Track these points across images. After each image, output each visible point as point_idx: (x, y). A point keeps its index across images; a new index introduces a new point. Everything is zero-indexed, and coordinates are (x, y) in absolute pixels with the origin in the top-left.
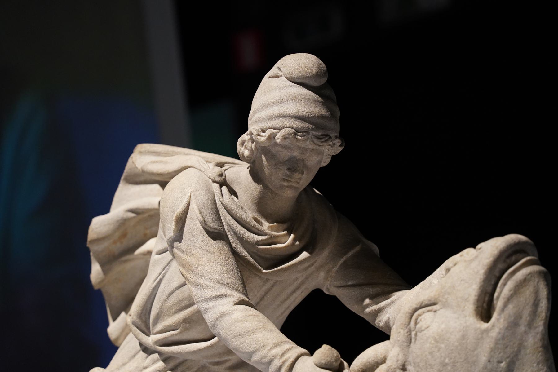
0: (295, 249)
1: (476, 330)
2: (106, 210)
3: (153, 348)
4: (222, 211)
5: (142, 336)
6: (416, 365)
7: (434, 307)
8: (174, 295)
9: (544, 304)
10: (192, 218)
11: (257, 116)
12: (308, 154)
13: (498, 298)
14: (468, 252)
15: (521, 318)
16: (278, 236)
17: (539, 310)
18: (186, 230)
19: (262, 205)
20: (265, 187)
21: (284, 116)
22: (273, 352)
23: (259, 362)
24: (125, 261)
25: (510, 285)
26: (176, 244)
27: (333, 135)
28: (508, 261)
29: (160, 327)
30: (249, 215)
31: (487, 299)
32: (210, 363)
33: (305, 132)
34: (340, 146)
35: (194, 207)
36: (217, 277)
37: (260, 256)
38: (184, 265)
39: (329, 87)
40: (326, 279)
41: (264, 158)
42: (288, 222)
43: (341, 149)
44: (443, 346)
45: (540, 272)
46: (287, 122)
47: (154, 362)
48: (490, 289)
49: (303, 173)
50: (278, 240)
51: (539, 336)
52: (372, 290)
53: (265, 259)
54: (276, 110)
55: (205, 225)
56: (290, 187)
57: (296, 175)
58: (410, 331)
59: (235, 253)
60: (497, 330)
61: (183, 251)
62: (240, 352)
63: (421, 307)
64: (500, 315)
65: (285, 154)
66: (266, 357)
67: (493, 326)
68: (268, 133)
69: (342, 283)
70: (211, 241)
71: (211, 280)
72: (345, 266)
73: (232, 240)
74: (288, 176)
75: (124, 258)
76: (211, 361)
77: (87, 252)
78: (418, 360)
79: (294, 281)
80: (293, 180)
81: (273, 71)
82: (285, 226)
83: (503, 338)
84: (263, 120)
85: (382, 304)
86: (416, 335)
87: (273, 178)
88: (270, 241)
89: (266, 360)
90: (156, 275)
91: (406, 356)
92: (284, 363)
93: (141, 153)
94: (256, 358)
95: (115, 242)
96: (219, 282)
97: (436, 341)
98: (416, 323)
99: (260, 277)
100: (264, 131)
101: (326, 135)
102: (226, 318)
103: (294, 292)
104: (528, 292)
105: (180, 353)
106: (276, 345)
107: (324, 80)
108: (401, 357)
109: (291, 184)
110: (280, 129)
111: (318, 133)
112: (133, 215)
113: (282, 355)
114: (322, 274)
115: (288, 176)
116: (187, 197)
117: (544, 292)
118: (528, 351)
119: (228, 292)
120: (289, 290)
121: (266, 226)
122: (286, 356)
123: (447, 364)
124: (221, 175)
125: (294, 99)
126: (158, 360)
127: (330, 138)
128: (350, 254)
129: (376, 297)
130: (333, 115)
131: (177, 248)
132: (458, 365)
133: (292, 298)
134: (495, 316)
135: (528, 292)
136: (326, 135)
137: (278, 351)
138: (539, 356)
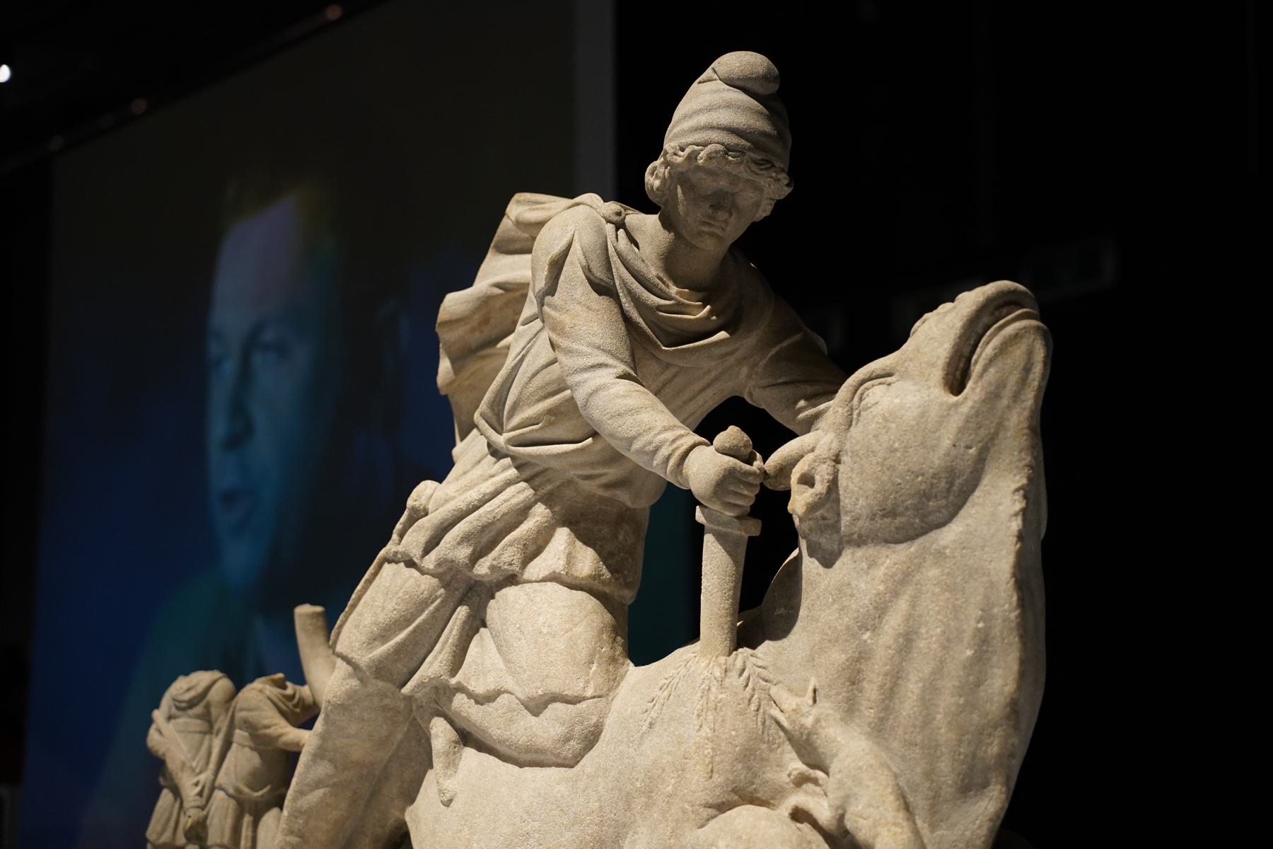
0: (710, 326)
1: (941, 404)
2: (467, 281)
3: (505, 451)
4: (615, 259)
5: (491, 432)
6: (855, 454)
7: (889, 379)
8: (539, 376)
9: (1038, 369)
10: (572, 263)
11: (675, 130)
12: (741, 186)
13: (976, 362)
14: (946, 306)
15: (1005, 387)
16: (689, 305)
17: (1031, 376)
18: (562, 278)
19: (669, 261)
20: (678, 236)
21: (712, 128)
22: (662, 437)
23: (641, 452)
24: (484, 357)
25: (996, 341)
26: (548, 299)
27: (778, 164)
28: (997, 313)
29: (516, 420)
30: (652, 271)
31: (961, 365)
32: (579, 476)
33: (740, 151)
34: (788, 185)
35: (576, 247)
36: (597, 341)
37: (659, 327)
38: (557, 328)
39: (777, 97)
40: (749, 377)
41: (679, 190)
42: (706, 291)
43: (788, 191)
44: (893, 426)
45: (1038, 328)
46: (715, 135)
47: (505, 469)
48: (967, 350)
49: (731, 214)
50: (688, 310)
51: (1026, 413)
52: (809, 389)
53: (667, 334)
54: (703, 119)
55: (588, 271)
56: (712, 235)
57: (722, 215)
58: (852, 409)
59: (627, 319)
60: (970, 403)
61: (555, 308)
62: (616, 438)
63: (870, 379)
64: (976, 383)
65: (710, 185)
66: (651, 443)
67: (966, 398)
68: (688, 150)
69: (771, 381)
70: (595, 295)
71: (589, 345)
72: (777, 358)
73: (623, 300)
74: (711, 217)
75: (483, 353)
76: (580, 472)
77: (434, 342)
78: (857, 447)
79: (705, 374)
80: (716, 224)
81: (708, 72)
82: (700, 295)
83: (977, 415)
84: (684, 133)
85: (822, 407)
86: (859, 414)
87: (690, 220)
88: (676, 309)
89: (651, 448)
90: (518, 350)
91: (841, 443)
92: (674, 451)
93: (518, 202)
94: (637, 445)
95: (473, 330)
96: (599, 348)
97: (886, 420)
98: (861, 399)
99: (658, 360)
100: (683, 150)
101: (768, 162)
102: (602, 393)
103: (703, 390)
104: (1018, 352)
105: (539, 456)
106: (666, 429)
107: (774, 87)
108: (835, 446)
109: (712, 229)
110: (705, 145)
111: (758, 157)
112: (501, 291)
113: (674, 441)
114: (745, 370)
115: (711, 217)
116: (569, 236)
117: (1040, 354)
118: (1009, 434)
119: (610, 361)
120: (697, 386)
121: (673, 290)
122: (678, 443)
123: (896, 450)
124: (619, 214)
125: (728, 105)
126: (509, 467)
127: (773, 166)
128: (785, 344)
129: (814, 398)
130: (780, 137)
131: (549, 305)
132: (911, 450)
133: (701, 399)
134: (970, 384)
135: (1019, 352)
136: (768, 162)
137: (669, 435)
138: (1024, 441)
